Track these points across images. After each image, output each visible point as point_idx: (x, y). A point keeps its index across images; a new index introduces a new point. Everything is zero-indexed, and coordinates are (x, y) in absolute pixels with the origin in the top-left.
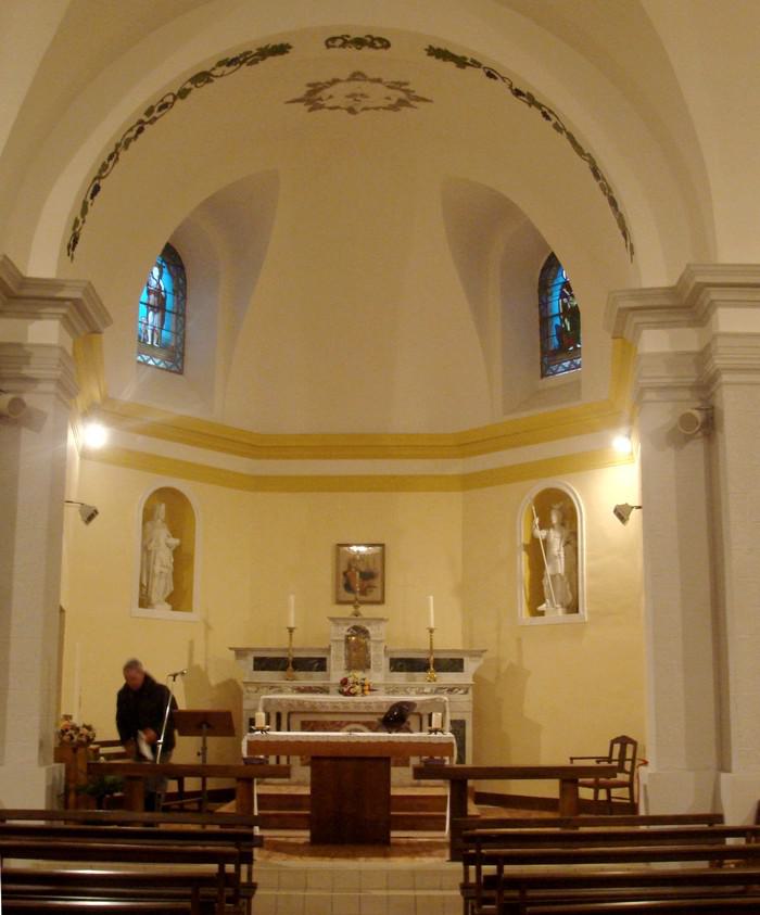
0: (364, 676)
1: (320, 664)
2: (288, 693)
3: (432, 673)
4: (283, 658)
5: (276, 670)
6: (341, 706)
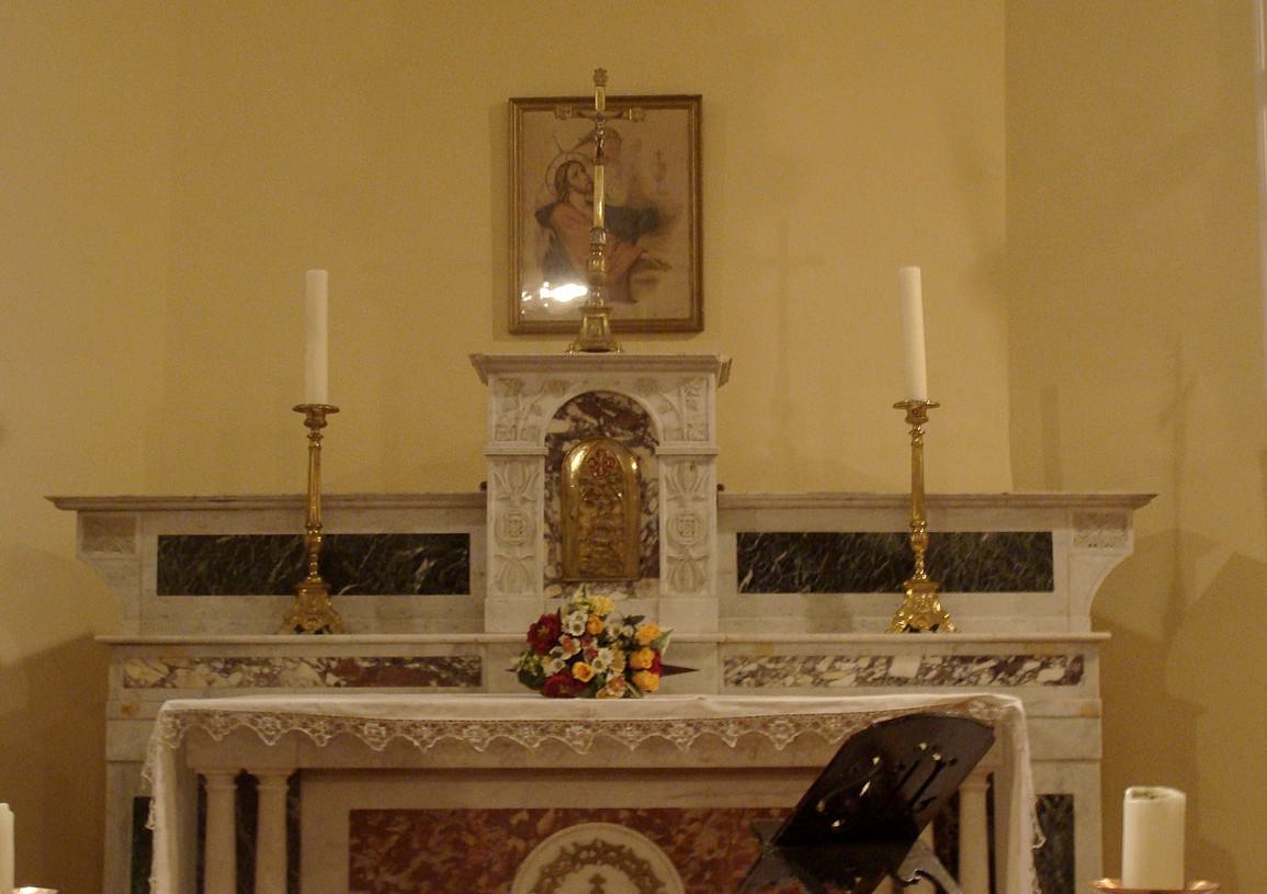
0: (633, 608)
1: (446, 566)
2: (301, 687)
3: (917, 596)
4: (284, 540)
5: (256, 591)
6: (524, 737)
